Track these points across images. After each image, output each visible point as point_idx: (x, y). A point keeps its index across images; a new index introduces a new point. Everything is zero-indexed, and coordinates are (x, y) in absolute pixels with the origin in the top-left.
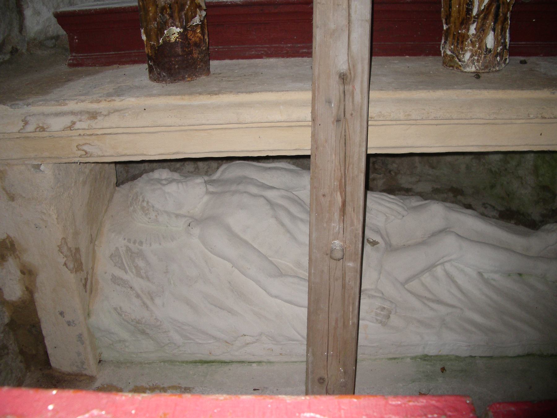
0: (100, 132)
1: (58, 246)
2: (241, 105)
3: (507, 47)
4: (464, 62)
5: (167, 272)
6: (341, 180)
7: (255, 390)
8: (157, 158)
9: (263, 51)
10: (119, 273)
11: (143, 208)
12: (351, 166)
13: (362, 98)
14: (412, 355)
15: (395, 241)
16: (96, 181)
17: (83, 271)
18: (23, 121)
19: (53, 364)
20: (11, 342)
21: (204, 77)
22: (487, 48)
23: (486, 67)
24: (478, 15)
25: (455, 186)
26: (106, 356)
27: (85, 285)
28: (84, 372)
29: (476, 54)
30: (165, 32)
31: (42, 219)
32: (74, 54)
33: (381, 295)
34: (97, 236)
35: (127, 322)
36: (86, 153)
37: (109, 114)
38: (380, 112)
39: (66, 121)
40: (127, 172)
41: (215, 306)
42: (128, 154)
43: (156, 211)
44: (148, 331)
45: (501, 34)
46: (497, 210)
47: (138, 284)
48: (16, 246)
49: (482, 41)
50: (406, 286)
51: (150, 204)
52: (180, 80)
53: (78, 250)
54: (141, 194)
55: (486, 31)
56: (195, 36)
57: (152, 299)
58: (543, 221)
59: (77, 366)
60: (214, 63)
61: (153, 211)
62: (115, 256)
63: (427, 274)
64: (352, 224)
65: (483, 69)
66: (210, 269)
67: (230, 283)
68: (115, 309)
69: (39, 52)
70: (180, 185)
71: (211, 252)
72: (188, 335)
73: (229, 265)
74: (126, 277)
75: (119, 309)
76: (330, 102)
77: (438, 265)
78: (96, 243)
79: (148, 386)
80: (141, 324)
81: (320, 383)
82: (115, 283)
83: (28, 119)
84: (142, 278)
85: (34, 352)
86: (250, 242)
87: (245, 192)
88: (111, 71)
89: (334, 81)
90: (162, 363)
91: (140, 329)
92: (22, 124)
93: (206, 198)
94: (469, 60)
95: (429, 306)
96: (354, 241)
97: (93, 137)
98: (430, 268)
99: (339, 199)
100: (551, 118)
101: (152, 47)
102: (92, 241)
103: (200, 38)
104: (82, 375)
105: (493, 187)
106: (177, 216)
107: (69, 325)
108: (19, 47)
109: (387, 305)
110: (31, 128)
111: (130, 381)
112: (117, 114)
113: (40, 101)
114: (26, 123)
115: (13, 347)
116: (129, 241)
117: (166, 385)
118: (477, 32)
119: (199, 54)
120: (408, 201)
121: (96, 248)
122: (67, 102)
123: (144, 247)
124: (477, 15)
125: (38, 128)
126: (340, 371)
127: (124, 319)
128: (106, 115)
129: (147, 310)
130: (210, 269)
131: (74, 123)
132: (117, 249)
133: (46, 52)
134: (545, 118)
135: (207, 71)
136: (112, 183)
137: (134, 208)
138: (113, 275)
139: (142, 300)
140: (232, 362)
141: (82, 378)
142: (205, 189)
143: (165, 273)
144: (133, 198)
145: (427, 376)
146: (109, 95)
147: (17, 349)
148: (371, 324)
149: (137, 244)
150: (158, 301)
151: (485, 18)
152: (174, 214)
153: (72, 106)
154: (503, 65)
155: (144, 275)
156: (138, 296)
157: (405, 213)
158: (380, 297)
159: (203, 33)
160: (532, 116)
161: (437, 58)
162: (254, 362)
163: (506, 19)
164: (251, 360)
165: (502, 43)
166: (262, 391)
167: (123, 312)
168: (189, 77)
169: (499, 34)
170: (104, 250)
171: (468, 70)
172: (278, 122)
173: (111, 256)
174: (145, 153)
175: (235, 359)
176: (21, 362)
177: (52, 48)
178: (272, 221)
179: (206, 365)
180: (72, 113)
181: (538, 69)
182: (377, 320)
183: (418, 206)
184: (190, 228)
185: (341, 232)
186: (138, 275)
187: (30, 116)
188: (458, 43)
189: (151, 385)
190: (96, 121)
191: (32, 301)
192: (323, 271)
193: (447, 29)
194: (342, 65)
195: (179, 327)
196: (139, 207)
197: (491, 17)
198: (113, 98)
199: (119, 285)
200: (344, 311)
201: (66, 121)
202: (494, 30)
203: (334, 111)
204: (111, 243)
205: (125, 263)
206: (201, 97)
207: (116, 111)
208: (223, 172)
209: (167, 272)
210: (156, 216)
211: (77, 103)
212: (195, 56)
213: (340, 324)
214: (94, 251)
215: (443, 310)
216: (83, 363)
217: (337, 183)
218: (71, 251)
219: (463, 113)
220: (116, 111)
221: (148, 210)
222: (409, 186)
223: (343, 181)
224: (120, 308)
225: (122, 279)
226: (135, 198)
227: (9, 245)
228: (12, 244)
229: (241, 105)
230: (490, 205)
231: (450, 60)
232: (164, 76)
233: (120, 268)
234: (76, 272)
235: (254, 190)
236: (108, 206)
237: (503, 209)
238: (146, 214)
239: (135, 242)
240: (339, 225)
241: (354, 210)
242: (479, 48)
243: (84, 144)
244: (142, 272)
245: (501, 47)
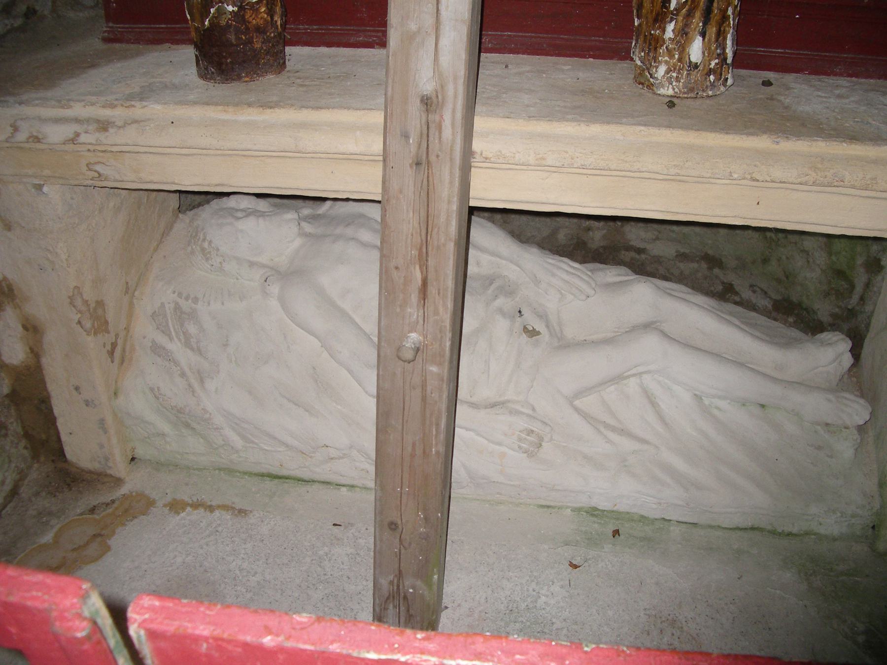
0: (115, 149)
1: (69, 297)
2: (303, 126)
3: (729, 61)
4: (657, 79)
6: (421, 249)
7: (335, 525)
8: (196, 189)
9: (376, 37)
10: (162, 340)
12: (436, 230)
13: (453, 134)
14: (575, 505)
15: (570, 332)
16: (139, 208)
17: (109, 333)
18: (11, 126)
19: (69, 455)
20: (12, 420)
21: (271, 77)
22: (690, 62)
23: (691, 90)
24: (678, 10)
25: (710, 252)
26: (140, 452)
27: (111, 353)
28: (109, 472)
29: (675, 69)
30: (212, 10)
31: (48, 259)
32: (111, 24)
33: (531, 412)
36: (100, 175)
37: (126, 124)
38: (500, 151)
39: (68, 131)
43: (222, 256)
44: (194, 425)
45: (717, 40)
46: (770, 298)
48: (16, 292)
49: (684, 49)
50: (577, 403)
52: (234, 80)
53: (100, 304)
54: (203, 229)
55: (690, 35)
56: (256, 16)
57: (202, 381)
58: (834, 325)
59: (100, 462)
60: (295, 54)
63: (612, 388)
64: (436, 313)
65: (685, 93)
66: (289, 347)
68: (152, 390)
69: (71, 14)
72: (250, 437)
74: (170, 346)
76: (406, 136)
77: (628, 377)
79: (190, 502)
81: (391, 529)
83: (19, 123)
84: (192, 349)
85: (44, 437)
88: (156, 54)
89: (415, 108)
90: (217, 472)
91: (183, 419)
92: (10, 130)
93: (298, 242)
94: (664, 76)
95: (605, 437)
96: (439, 336)
97: (109, 154)
98: (618, 379)
99: (418, 275)
100: (767, 181)
101: (197, 29)
103: (265, 20)
104: (106, 475)
105: (765, 261)
106: (252, 264)
107: (87, 405)
108: (37, 8)
109: (536, 427)
110: (21, 136)
111: (168, 491)
112: (135, 126)
113: (37, 99)
114: (16, 129)
115: (15, 427)
116: (180, 295)
117: (214, 503)
118: (676, 36)
119: (263, 43)
120: (600, 273)
121: (135, 301)
122: (72, 104)
123: (199, 306)
124: (675, 9)
125: (30, 137)
126: (419, 516)
128: (120, 127)
131: (78, 135)
132: (163, 304)
133: (81, 14)
134: (758, 181)
135: (280, 65)
136: (171, 209)
138: (153, 341)
140: (313, 481)
141: (106, 480)
145: (588, 539)
146: (130, 97)
147: (20, 430)
148: (511, 452)
149: (190, 301)
150: (211, 385)
151: (690, 15)
153: (78, 110)
154: (722, 89)
155: (195, 346)
156: (183, 375)
157: (591, 292)
158: (529, 416)
159: (271, 12)
160: (735, 176)
161: (625, 64)
162: (344, 486)
163: (724, 18)
164: (339, 482)
165: (719, 55)
166: (346, 527)
168: (247, 76)
169: (713, 40)
170: (145, 306)
171: (662, 91)
172: (352, 154)
173: (154, 315)
175: (316, 477)
176: (26, 448)
177: (92, 7)
179: (276, 481)
180: (77, 120)
181: (782, 98)
182: (520, 447)
183: (615, 283)
184: (266, 284)
185: (421, 322)
186: (187, 344)
187: (22, 119)
188: (650, 50)
189: (195, 500)
190: (107, 134)
191: (39, 368)
192: (395, 373)
193: (640, 25)
194: (426, 84)
195: (237, 424)
197: (698, 14)
198: (133, 103)
200: (424, 434)
201: (68, 131)
202: (703, 35)
203: (413, 149)
204: (158, 295)
205: (171, 326)
206: (250, 110)
207: (136, 121)
211: (84, 106)
212: (257, 46)
213: (419, 452)
214: (131, 305)
215: (627, 445)
216: (107, 459)
217: (415, 252)
218: (88, 305)
219: (626, 162)
220: (136, 121)
221: (209, 253)
222: (641, 245)
223: (424, 250)
224: (158, 388)
225: (164, 348)
227: (6, 289)
228: (11, 289)
229: (303, 126)
230: (762, 290)
231: (640, 74)
232: (213, 73)
233: (163, 332)
234: (95, 334)
237: (778, 297)
238: (207, 259)
239: (187, 299)
240: (418, 310)
241: (439, 294)
242: (680, 60)
243: (96, 163)
244: (193, 341)
245: (717, 61)
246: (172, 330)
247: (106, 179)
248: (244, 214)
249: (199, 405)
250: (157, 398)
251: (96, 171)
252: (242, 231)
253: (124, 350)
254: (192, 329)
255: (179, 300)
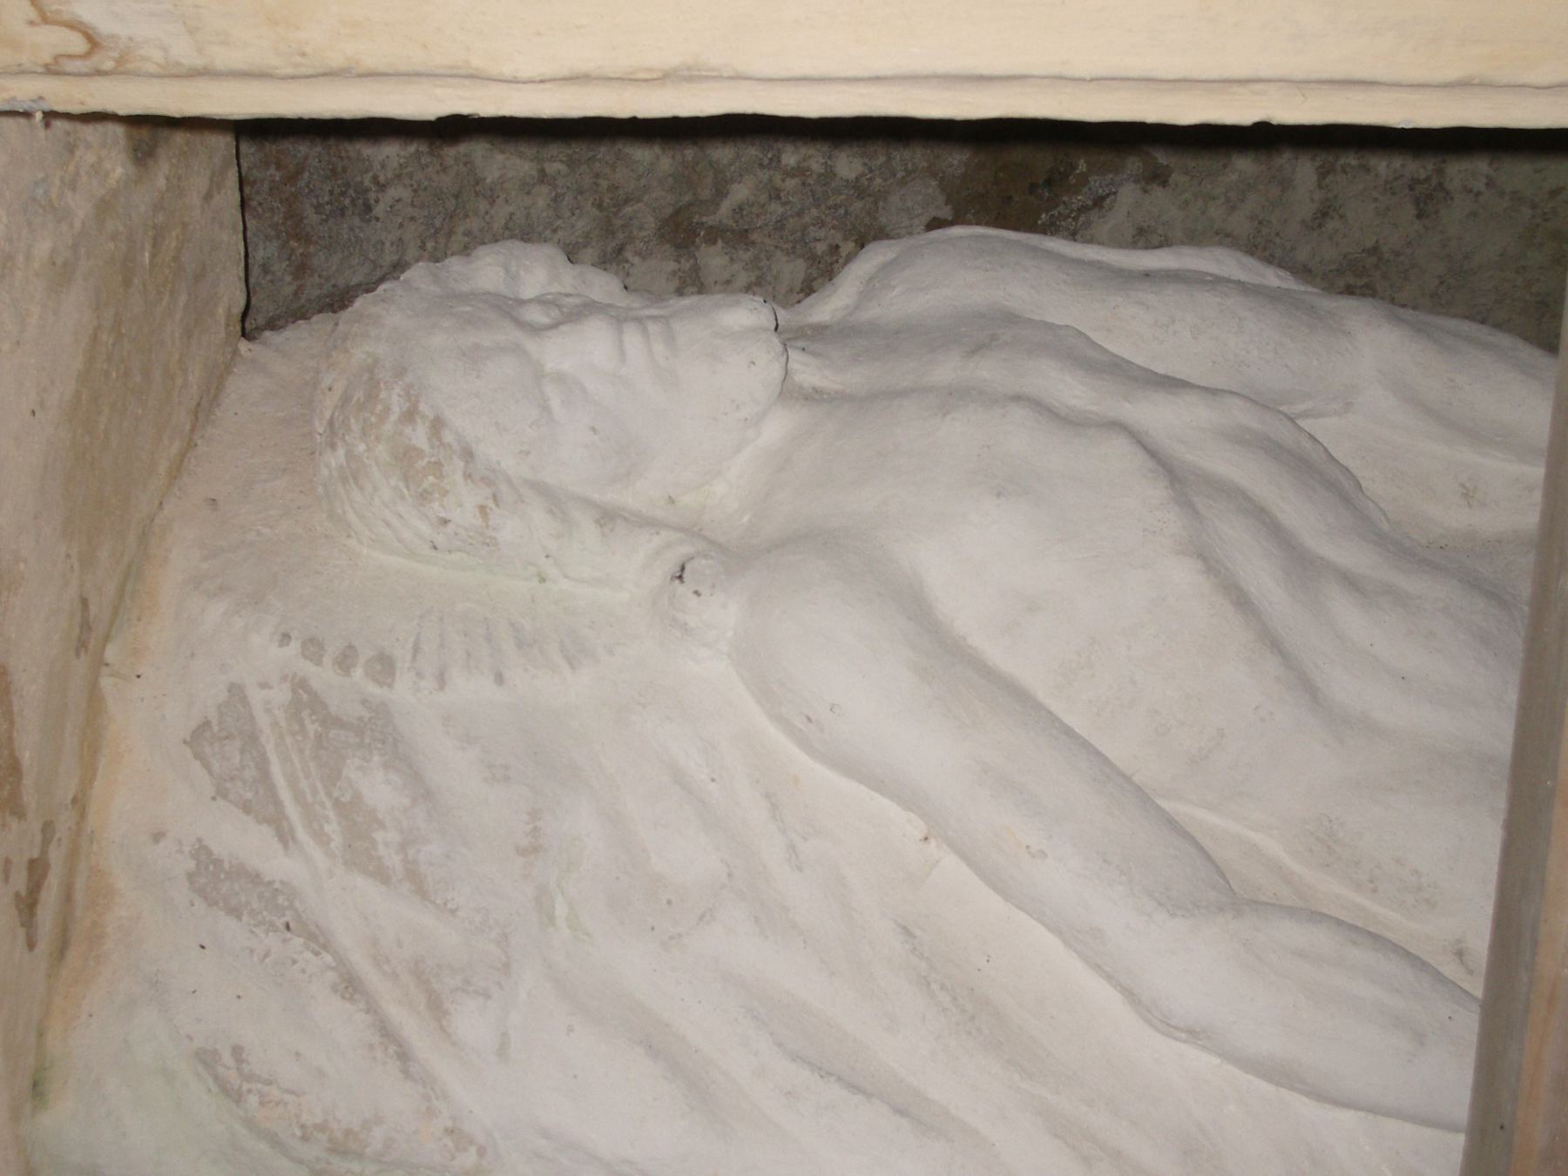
5: (532, 849)
10: (242, 840)
11: (405, 457)
16: (127, 282)
17: (19, 812)
27: (28, 905)
34: (116, 610)
35: (275, 1142)
36: (94, 42)
40: (301, 269)
41: (824, 1073)
42: (370, 62)
47: (354, 908)
51: (448, 437)
54: (400, 372)
57: (437, 1008)
61: (468, 476)
62: (222, 737)
66: (792, 847)
67: (907, 931)
68: (206, 1059)
70: (632, 336)
71: (805, 744)
73: (914, 827)
74: (278, 865)
75: (227, 1058)
78: (111, 653)
80: (360, 1156)
82: (212, 903)
84: (382, 875)
86: (1041, 696)
87: (1018, 398)
93: (778, 427)
102: (89, 635)
106: (608, 517)
116: (313, 648)
121: (106, 683)
127: (250, 1123)
129: (406, 1073)
130: (792, 847)
132: (236, 691)
137: (350, 455)
138: (202, 852)
139: (372, 1009)
142: (776, 372)
143: (521, 852)
144: (346, 399)
149: (358, 673)
150: (472, 1022)
152: (588, 503)
155: (394, 860)
156: (350, 986)
167: (250, 1078)
170: (152, 710)
173: (199, 736)
174: (477, 62)
178: (1184, 575)
186: (359, 855)
196: (381, 450)
199: (235, 912)
204: (206, 649)
208: (869, 291)
209: (532, 849)
210: (483, 509)
214: (94, 699)
224: (237, 1051)
225: (256, 878)
226: (359, 395)
233: (246, 808)
235: (1072, 390)
236: (191, 445)
239: (345, 661)
244: (386, 841)
246: (285, 795)
247: (122, 69)
248: (555, 313)
249: (431, 1113)
250: (238, 1098)
251: (74, 25)
252: (560, 378)
253: (68, 897)
254: (378, 788)
255: (307, 668)
